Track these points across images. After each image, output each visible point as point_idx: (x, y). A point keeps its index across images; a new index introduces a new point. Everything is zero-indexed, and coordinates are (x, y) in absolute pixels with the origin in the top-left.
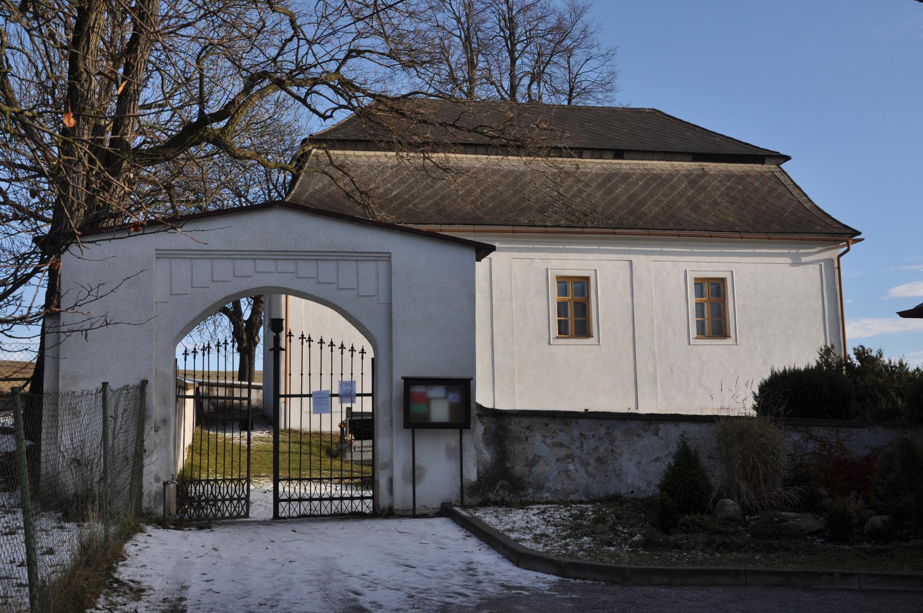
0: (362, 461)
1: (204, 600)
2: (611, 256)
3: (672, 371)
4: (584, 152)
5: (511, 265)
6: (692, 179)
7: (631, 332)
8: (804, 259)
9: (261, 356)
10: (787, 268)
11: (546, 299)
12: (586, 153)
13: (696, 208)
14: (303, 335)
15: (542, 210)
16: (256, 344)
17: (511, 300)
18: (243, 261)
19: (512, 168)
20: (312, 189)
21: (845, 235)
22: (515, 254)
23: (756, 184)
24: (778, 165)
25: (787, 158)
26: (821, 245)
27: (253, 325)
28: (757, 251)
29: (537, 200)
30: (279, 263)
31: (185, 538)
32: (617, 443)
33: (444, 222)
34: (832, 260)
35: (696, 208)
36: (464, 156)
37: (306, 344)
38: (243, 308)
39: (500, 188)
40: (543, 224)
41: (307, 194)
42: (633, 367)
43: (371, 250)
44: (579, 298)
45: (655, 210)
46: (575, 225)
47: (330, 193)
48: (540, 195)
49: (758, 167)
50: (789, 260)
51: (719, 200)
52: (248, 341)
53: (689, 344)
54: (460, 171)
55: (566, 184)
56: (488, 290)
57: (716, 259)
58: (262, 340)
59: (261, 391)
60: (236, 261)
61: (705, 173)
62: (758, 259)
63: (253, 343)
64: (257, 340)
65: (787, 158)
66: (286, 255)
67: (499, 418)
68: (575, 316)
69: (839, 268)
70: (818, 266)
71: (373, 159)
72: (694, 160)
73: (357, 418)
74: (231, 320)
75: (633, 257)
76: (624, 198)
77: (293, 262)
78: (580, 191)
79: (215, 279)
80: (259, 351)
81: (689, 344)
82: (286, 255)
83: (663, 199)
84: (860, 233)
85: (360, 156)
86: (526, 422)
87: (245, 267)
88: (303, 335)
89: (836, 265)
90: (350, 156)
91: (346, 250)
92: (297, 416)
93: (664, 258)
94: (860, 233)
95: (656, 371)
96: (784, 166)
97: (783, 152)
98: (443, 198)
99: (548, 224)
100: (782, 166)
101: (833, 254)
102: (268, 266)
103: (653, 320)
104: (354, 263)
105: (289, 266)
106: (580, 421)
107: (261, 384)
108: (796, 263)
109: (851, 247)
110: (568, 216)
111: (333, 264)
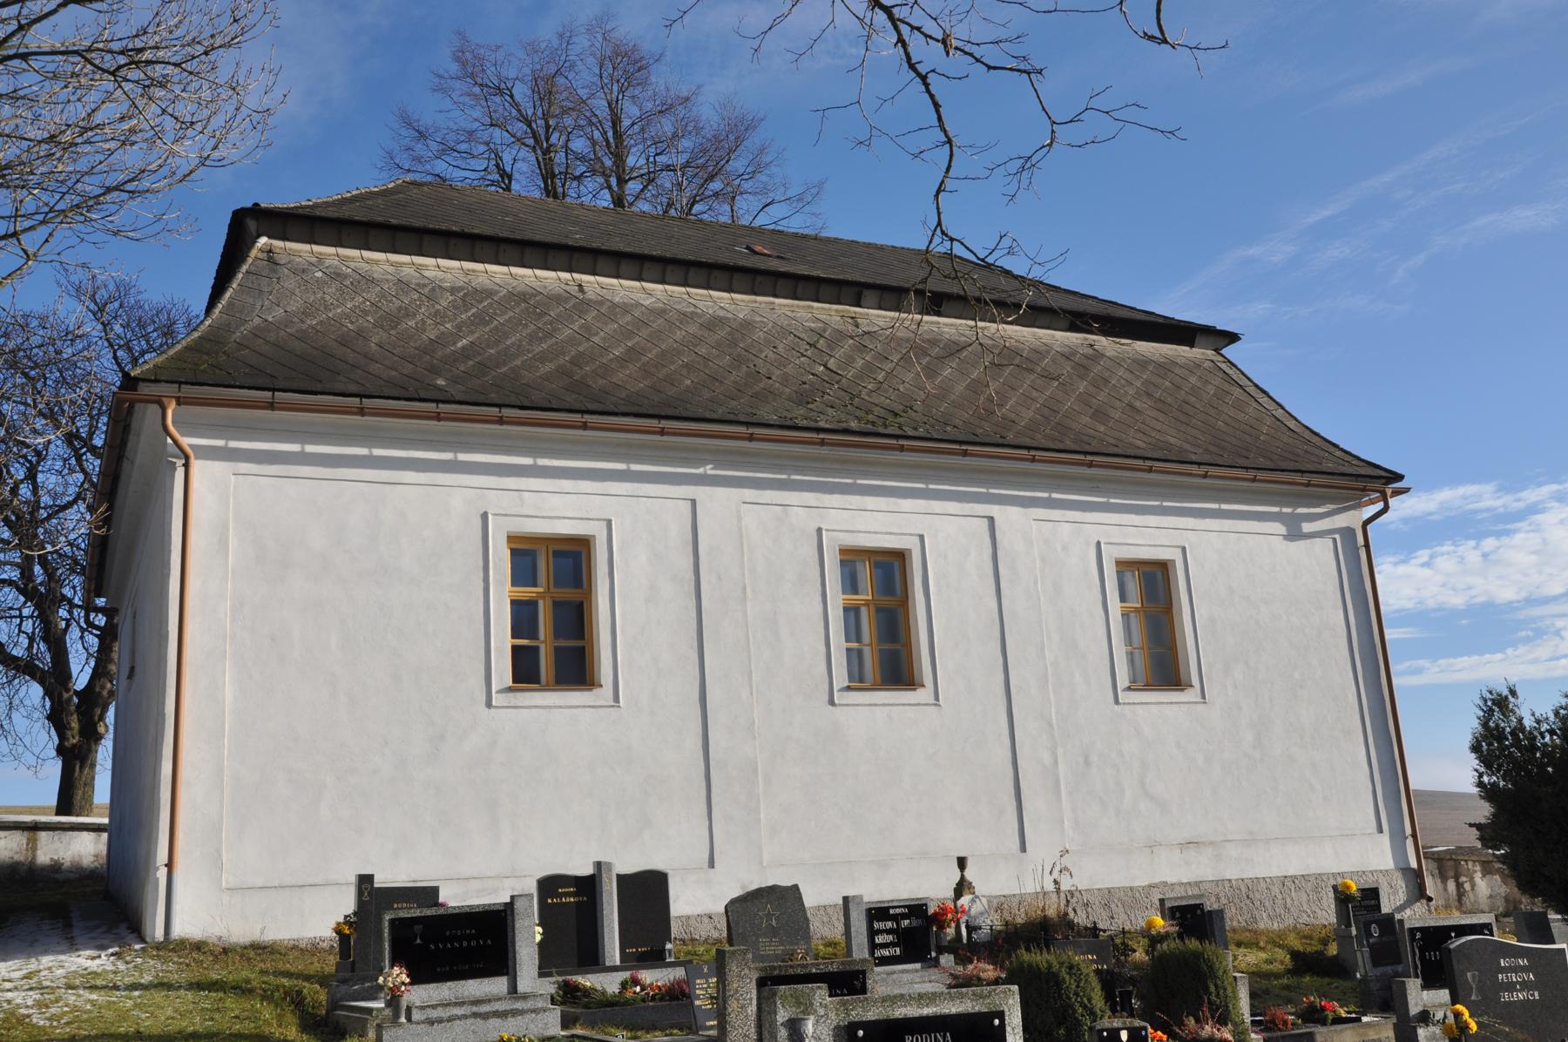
1: (328, 262)
2: (952, 507)
3: (1087, 763)
4: (866, 292)
5: (740, 519)
6: (1084, 364)
7: (1001, 677)
8: (1307, 527)
9: (109, 764)
10: (1279, 544)
11: (819, 598)
12: (869, 296)
13: (1100, 415)
15: (803, 399)
16: (98, 738)
17: (744, 599)
19: (722, 313)
20: (257, 321)
21: (1379, 482)
22: (749, 494)
23: (1193, 380)
24: (1217, 350)
25: (1232, 338)
26: (1332, 500)
27: (91, 700)
28: (1224, 506)
29: (785, 379)
33: (590, 406)
34: (1348, 533)
35: (1100, 415)
36: (614, 281)
38: (75, 668)
39: (703, 351)
40: (812, 424)
41: (244, 330)
42: (1009, 754)
44: (887, 601)
45: (1028, 414)
46: (881, 430)
47: (304, 331)
48: (790, 369)
49: (1183, 351)
50: (1280, 528)
51: (1138, 404)
52: (82, 733)
53: (1117, 702)
54: (615, 310)
55: (839, 353)
56: (690, 575)
57: (1152, 520)
58: (111, 728)
59: (105, 836)
61: (1097, 356)
62: (1228, 524)
63: (91, 735)
64: (101, 729)
65: (1232, 338)
68: (881, 640)
69: (1367, 546)
70: (1330, 542)
71: (407, 271)
72: (1073, 328)
74: (48, 692)
75: (994, 510)
76: (960, 388)
78: (869, 368)
80: (104, 753)
81: (1117, 702)
83: (1035, 394)
84: (1400, 477)
85: (377, 262)
89: (1361, 541)
90: (353, 259)
92: (199, 901)
93: (1056, 514)
94: (1400, 477)
95: (1056, 762)
96: (1230, 351)
98: (576, 361)
99: (822, 424)
101: (1352, 518)
103: (1042, 649)
107: (106, 821)
108: (1294, 535)
109: (1392, 502)
110: (858, 413)
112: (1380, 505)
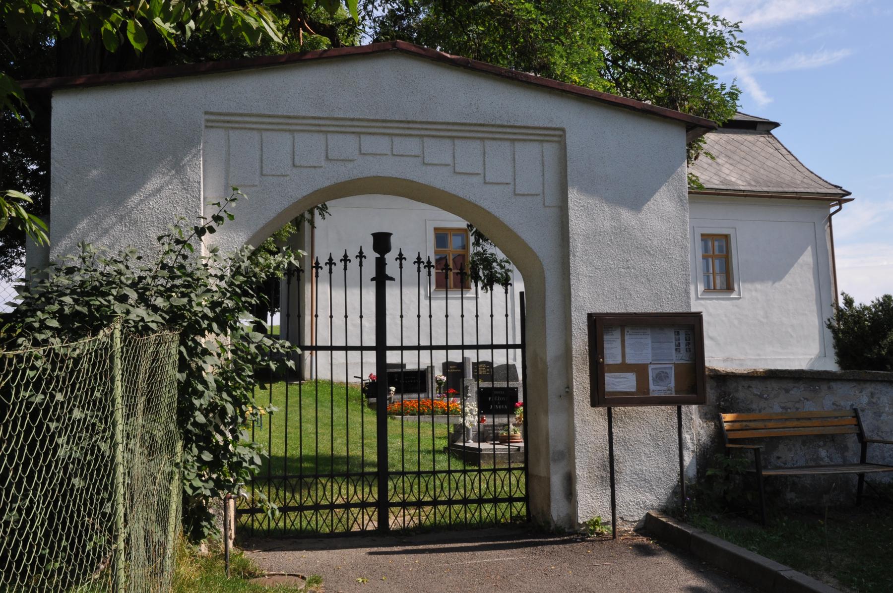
0: (509, 443)
14: (419, 258)
18: (341, 136)
25: (776, 125)
30: (397, 140)
31: (787, 391)
32: (884, 417)
37: (424, 271)
43: (536, 124)
60: (329, 136)
65: (776, 125)
66: (409, 127)
67: (723, 379)
73: (396, 370)
77: (417, 140)
79: (297, 163)
82: (409, 127)
84: (849, 194)
86: (758, 388)
87: (345, 145)
88: (419, 258)
91: (498, 122)
94: (849, 194)
97: (772, 119)
100: (772, 132)
102: (381, 144)
104: (507, 144)
105: (411, 146)
106: (833, 384)
111: (477, 144)
112: (838, 207)
